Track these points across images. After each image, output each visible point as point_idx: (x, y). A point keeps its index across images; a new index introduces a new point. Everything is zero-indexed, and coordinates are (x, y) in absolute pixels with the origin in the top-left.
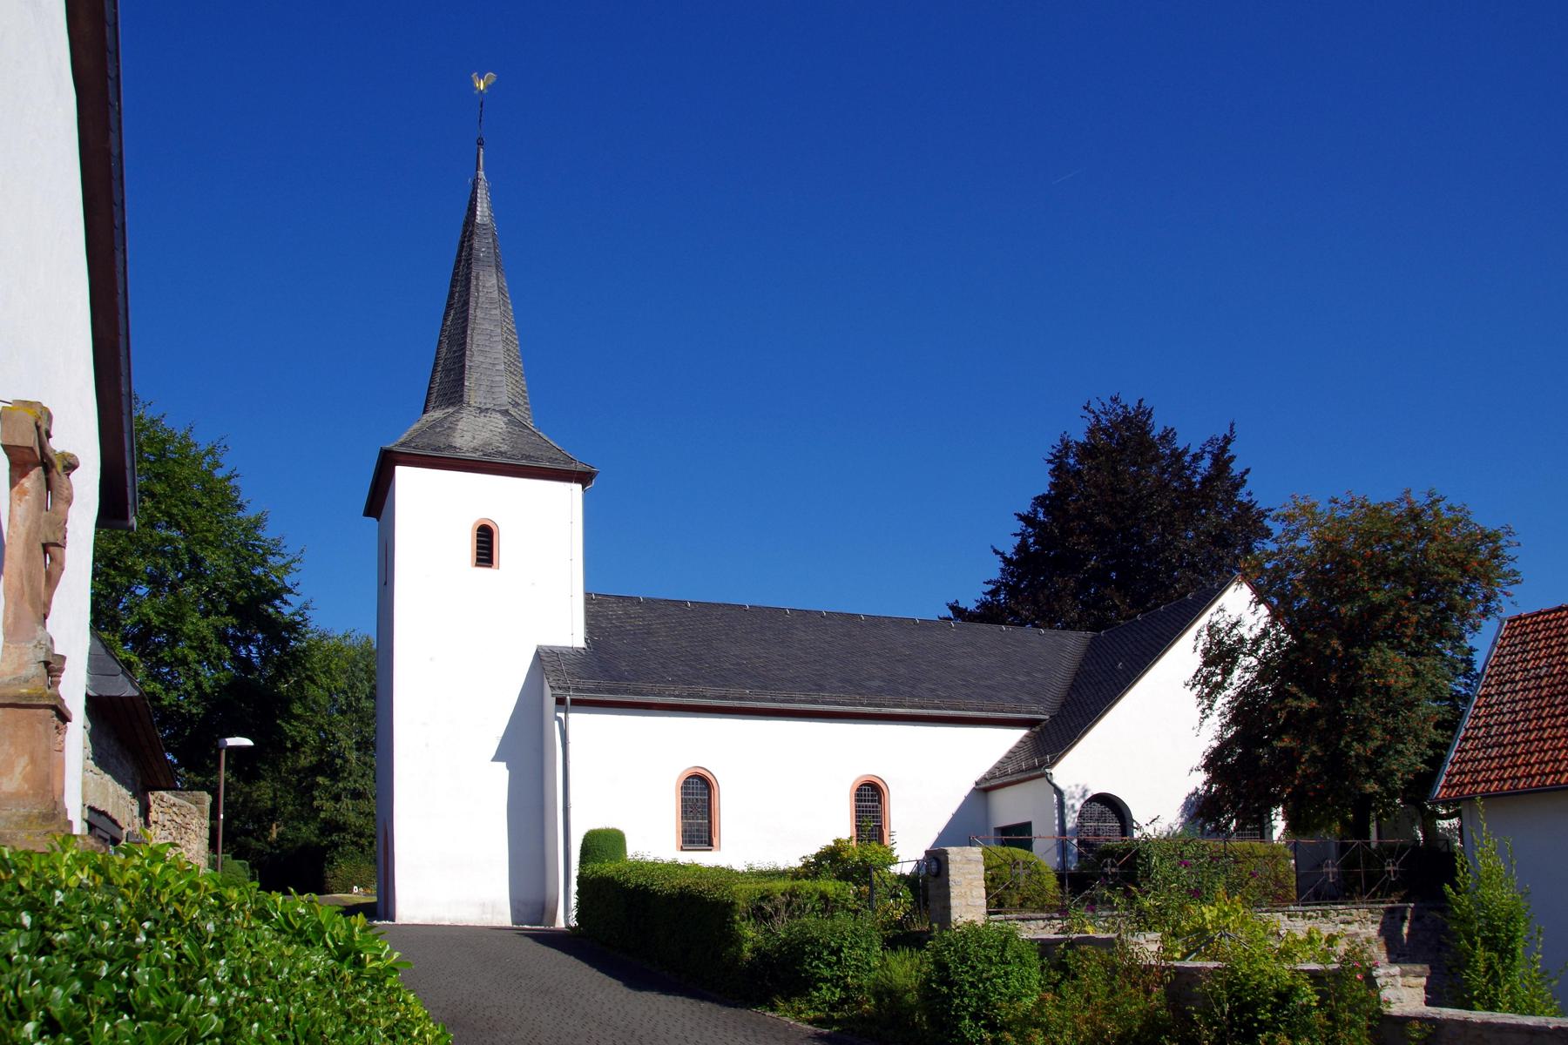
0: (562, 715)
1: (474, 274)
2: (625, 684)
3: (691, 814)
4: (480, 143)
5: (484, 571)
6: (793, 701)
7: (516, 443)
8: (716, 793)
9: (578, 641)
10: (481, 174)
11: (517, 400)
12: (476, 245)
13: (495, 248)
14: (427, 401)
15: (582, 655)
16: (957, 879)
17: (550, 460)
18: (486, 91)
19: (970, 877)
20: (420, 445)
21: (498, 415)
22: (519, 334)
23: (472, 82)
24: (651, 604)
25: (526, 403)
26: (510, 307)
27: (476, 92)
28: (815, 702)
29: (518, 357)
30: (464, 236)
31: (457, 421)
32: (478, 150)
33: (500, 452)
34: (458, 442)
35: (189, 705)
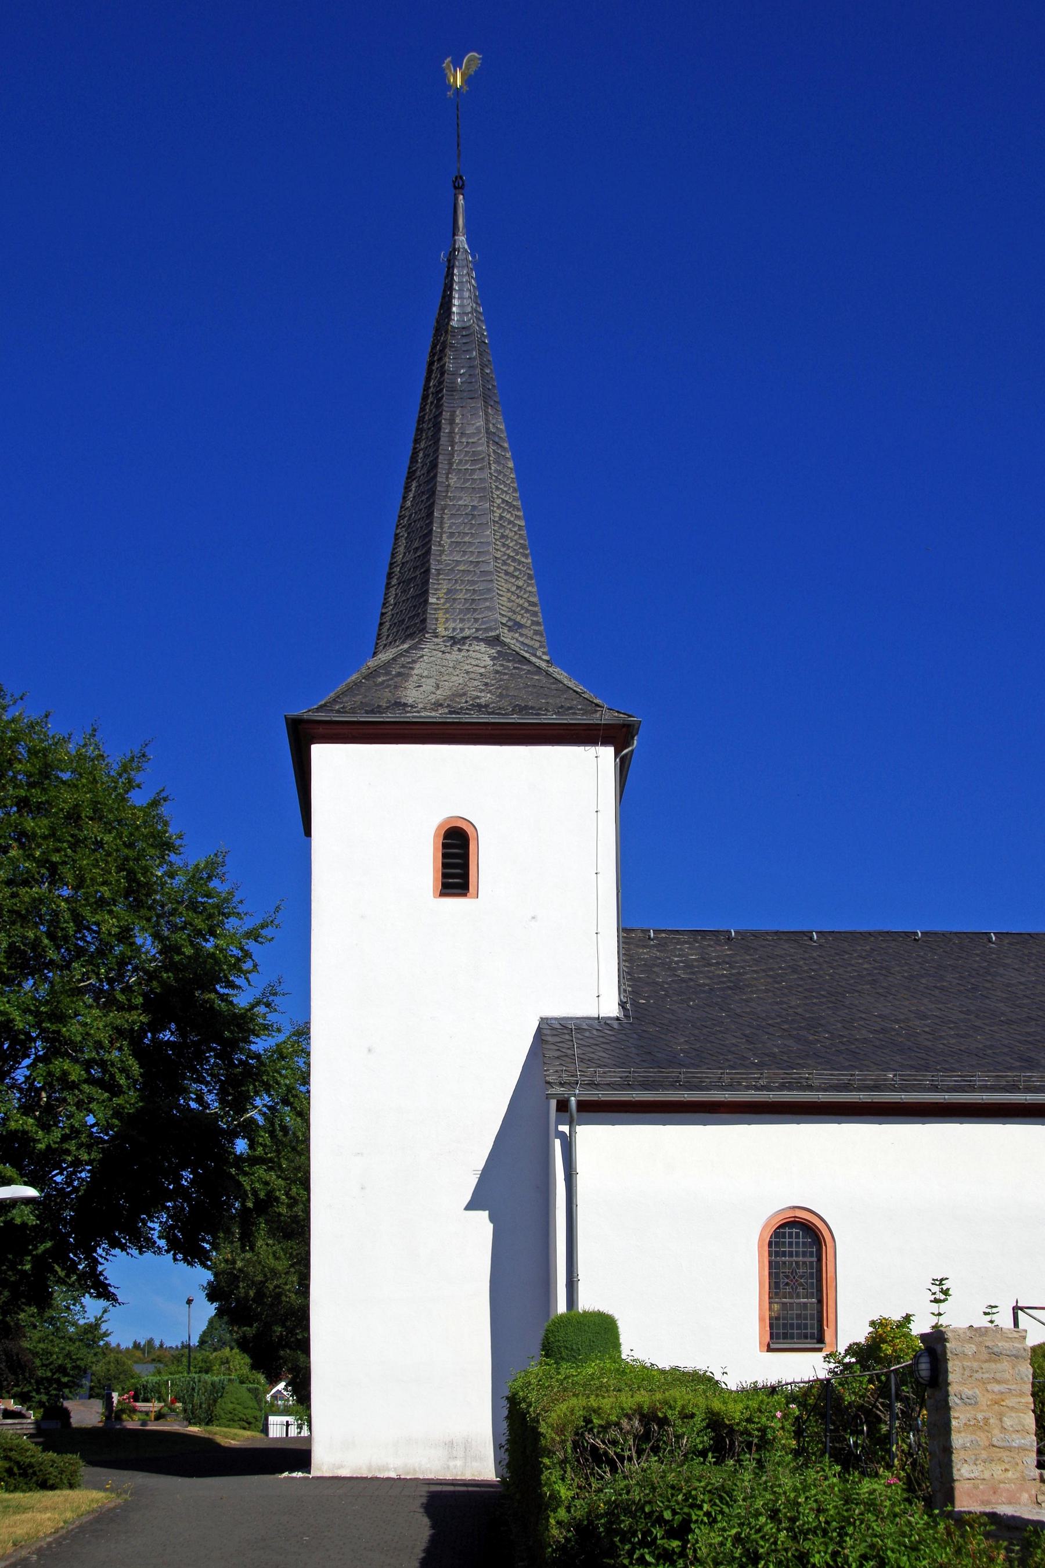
0: (564, 1128)
1: (446, 415)
2: (673, 1072)
3: (788, 1289)
4: (458, 186)
5: (454, 904)
6: (972, 1089)
7: (507, 688)
8: (830, 1251)
9: (610, 1007)
10: (462, 240)
11: (518, 618)
12: (450, 366)
13: (483, 366)
14: (379, 637)
15: (612, 1029)
16: (967, 1392)
17: (561, 710)
18: (466, 88)
19: (997, 1388)
20: (349, 706)
21: (482, 647)
22: (525, 507)
23: (444, 77)
24: (748, 940)
25: (534, 623)
26: (511, 464)
27: (450, 94)
28: (1013, 1088)
29: (523, 546)
30: (432, 354)
31: (414, 662)
32: (456, 199)
33: (480, 706)
34: (411, 695)
35: (78, 1149)
